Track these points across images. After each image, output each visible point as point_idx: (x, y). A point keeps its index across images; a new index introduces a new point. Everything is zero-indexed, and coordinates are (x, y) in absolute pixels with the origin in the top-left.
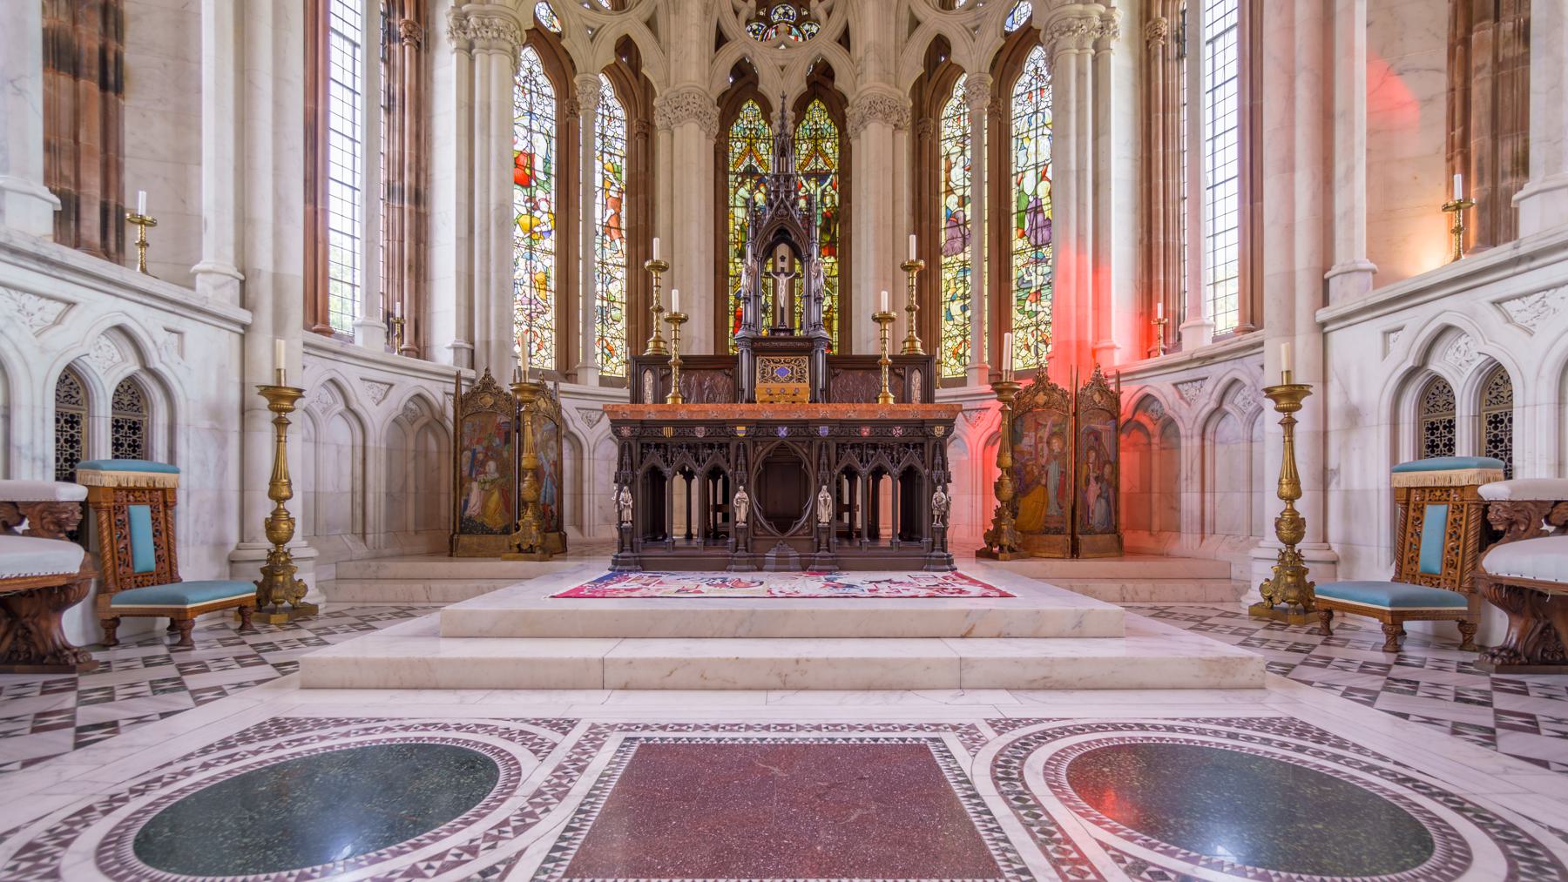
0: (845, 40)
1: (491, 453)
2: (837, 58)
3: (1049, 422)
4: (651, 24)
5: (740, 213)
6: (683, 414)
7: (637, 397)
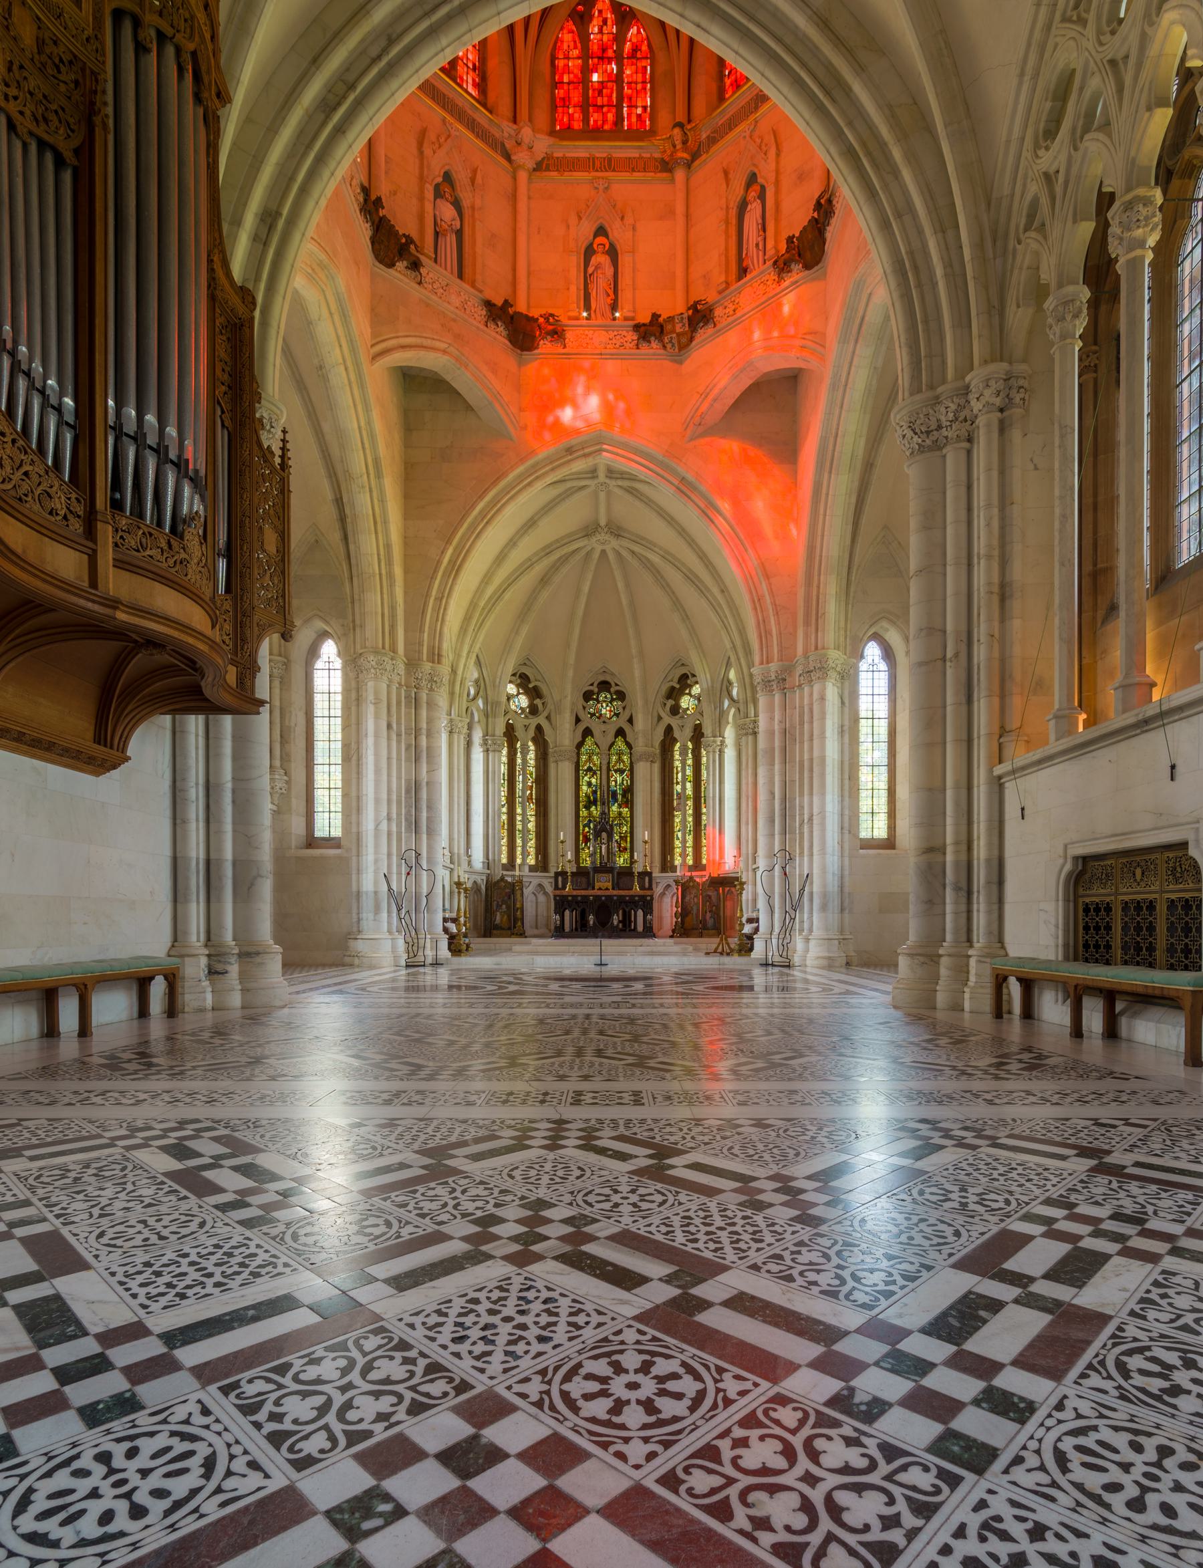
0: (630, 721)
1: (503, 902)
2: (627, 728)
3: (694, 891)
4: (548, 718)
5: (585, 788)
6: (575, 893)
7: (556, 888)
